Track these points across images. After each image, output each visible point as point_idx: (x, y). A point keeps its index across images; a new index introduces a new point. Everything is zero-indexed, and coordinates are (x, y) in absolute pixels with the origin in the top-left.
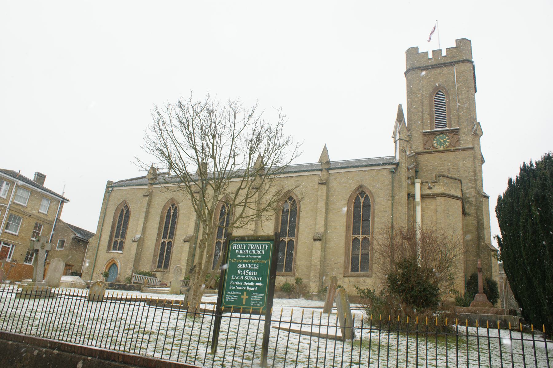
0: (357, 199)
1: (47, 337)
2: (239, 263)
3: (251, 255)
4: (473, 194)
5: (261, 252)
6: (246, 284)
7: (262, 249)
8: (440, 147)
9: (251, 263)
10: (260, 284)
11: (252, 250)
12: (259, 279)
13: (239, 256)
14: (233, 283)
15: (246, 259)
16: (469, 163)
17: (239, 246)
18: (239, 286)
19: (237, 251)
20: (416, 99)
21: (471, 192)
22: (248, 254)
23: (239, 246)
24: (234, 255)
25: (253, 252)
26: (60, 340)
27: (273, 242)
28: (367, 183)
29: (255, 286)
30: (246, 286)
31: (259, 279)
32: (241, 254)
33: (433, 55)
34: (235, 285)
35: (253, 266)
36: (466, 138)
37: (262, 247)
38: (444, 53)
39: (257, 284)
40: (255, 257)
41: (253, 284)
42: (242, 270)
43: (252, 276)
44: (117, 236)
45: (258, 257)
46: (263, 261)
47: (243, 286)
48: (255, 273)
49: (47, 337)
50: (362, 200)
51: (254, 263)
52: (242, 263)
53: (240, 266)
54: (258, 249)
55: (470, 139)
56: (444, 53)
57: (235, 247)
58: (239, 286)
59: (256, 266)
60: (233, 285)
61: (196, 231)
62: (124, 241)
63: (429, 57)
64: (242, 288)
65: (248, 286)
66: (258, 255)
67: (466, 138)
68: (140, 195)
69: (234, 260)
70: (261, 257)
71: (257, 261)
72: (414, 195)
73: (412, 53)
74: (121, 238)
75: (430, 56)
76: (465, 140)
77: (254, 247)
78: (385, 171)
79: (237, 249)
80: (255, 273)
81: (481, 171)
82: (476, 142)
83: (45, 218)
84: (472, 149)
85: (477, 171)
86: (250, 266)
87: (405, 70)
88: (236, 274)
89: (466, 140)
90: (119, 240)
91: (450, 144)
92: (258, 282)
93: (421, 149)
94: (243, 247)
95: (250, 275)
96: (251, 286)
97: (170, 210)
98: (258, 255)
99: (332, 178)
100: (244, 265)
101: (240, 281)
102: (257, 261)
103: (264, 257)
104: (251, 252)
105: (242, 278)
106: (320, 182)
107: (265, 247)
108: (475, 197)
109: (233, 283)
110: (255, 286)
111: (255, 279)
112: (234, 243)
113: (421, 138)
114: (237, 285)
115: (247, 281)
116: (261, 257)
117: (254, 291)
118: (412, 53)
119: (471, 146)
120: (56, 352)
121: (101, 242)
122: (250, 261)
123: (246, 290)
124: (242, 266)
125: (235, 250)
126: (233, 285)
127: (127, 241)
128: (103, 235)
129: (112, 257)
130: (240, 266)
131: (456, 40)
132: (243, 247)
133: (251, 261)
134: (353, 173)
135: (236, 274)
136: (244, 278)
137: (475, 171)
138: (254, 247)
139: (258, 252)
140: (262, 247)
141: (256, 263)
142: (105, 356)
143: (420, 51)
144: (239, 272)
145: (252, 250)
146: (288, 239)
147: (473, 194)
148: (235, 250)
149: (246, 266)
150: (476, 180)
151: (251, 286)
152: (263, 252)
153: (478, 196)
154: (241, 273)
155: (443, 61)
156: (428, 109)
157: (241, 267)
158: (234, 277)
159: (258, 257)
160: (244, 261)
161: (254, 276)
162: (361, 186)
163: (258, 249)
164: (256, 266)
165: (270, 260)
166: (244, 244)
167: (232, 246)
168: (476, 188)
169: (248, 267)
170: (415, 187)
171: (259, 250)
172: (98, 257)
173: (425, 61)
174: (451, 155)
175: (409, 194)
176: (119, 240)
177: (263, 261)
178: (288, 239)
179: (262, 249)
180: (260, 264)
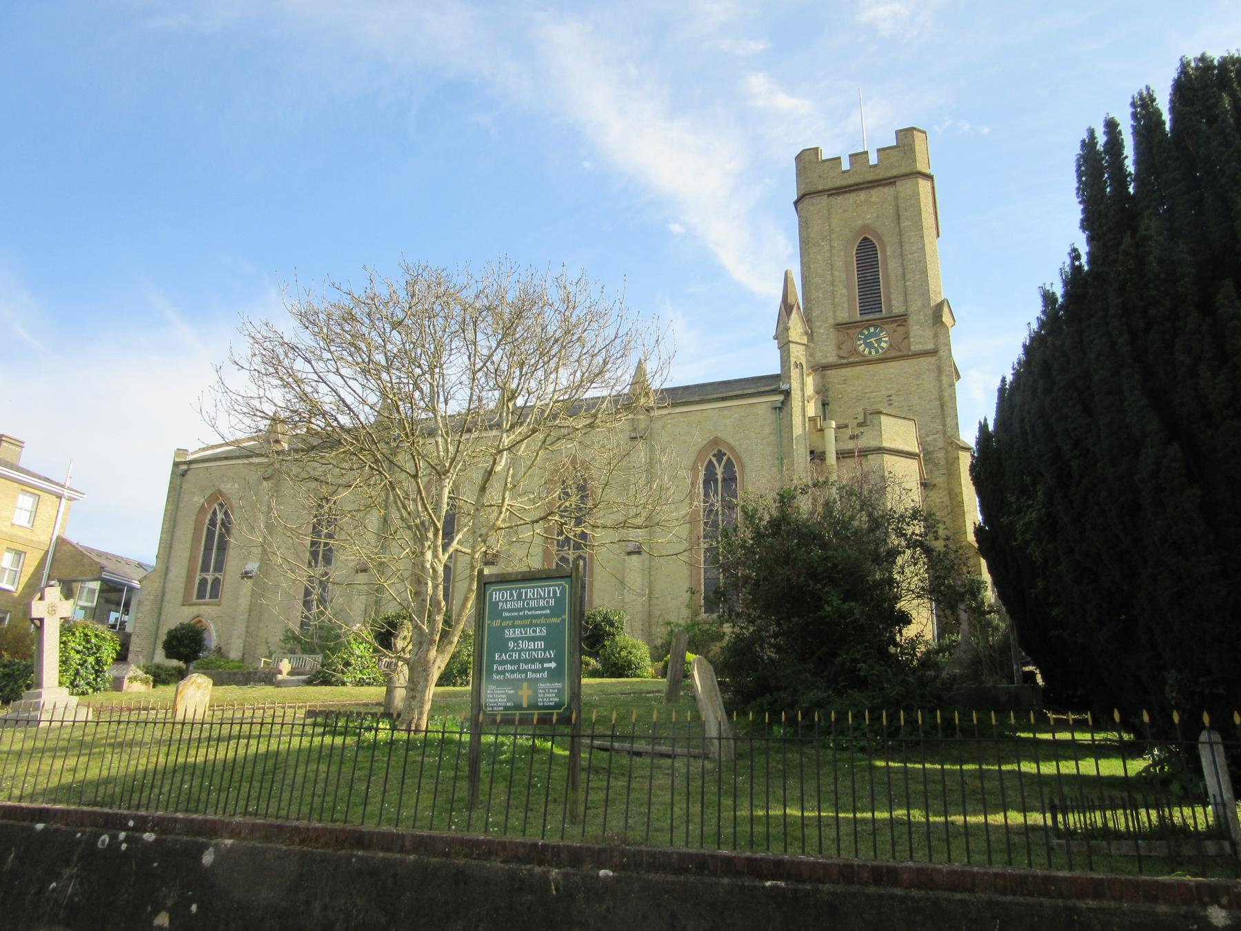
0: (710, 467)
1: (256, 814)
2: (509, 627)
3: (529, 609)
4: (941, 444)
5: (548, 603)
6: (525, 667)
7: (549, 597)
8: (870, 353)
9: (531, 626)
10: (553, 665)
11: (531, 599)
12: (550, 655)
13: (506, 614)
14: (500, 668)
15: (519, 618)
16: (929, 383)
17: (503, 594)
18: (512, 672)
19: (500, 604)
20: (819, 257)
21: (935, 440)
22: (524, 609)
23: (503, 594)
24: (496, 613)
25: (532, 604)
26: (250, 814)
27: (569, 580)
28: (229, 488)
29: (543, 670)
30: (525, 671)
31: (550, 655)
32: (509, 611)
33: (851, 164)
34: (503, 672)
35: (534, 631)
36: (922, 333)
37: (549, 592)
38: (873, 159)
39: (546, 665)
40: (538, 612)
41: (538, 666)
42: (516, 640)
43: (535, 650)
44: (205, 568)
45: (544, 612)
46: (554, 620)
47: (519, 671)
48: (541, 644)
49: (287, 818)
50: (719, 471)
51: (536, 625)
52: (514, 627)
53: (509, 633)
54: (541, 598)
55: (929, 333)
56: (873, 159)
57: (496, 596)
58: (512, 672)
59: (541, 630)
60: (499, 673)
61: (572, 632)
62: (221, 578)
63: (844, 169)
64: (519, 676)
65: (529, 670)
66: (543, 608)
67: (922, 333)
68: (253, 477)
69: (496, 623)
70: (548, 612)
71: (542, 620)
72: (824, 453)
73: (807, 161)
74: (215, 570)
75: (846, 166)
76: (920, 336)
77: (533, 594)
78: (764, 406)
79: (500, 601)
80: (541, 644)
81: (953, 398)
82: (942, 340)
83: (29, 537)
84: (934, 352)
85: (946, 399)
86: (530, 632)
87: (795, 198)
88: (505, 649)
89: (921, 336)
90: (210, 577)
91: (891, 345)
92: (549, 661)
93: (832, 359)
94: (511, 595)
95: (532, 650)
96: (534, 671)
97: (215, 513)
98: (543, 608)
99: (657, 425)
100: (517, 631)
101: (512, 662)
102: (542, 620)
103: (556, 611)
104: (528, 604)
105: (515, 656)
106: (633, 435)
107: (555, 592)
108: (943, 451)
109: (500, 668)
110: (543, 670)
111: (541, 655)
112: (494, 590)
113: (832, 336)
114: (508, 671)
115: (526, 662)
116: (548, 612)
117: (541, 680)
118: (807, 161)
119: (930, 346)
120: (40, 826)
121: (169, 585)
122: (527, 622)
123: (526, 679)
124: (515, 632)
125: (497, 603)
126: (499, 673)
127: (228, 578)
128: (171, 568)
129: (196, 613)
130: (509, 633)
131: (897, 132)
132: (511, 595)
133: (529, 620)
134: (699, 413)
135: (505, 649)
136: (520, 655)
137: (941, 398)
138: (533, 594)
139: (541, 603)
140: (549, 592)
141: (542, 625)
142: (408, 844)
143: (826, 155)
144: (511, 645)
145: (531, 599)
146: (574, 553)
147: (941, 444)
148: (497, 603)
149: (521, 632)
150: (943, 416)
151: (534, 671)
152: (552, 602)
153: (950, 448)
154: (514, 646)
155: (871, 177)
156: (844, 276)
157: (511, 636)
158: (500, 656)
159: (544, 612)
160: (517, 622)
161: (538, 650)
162: (716, 441)
163: (541, 598)
164: (541, 630)
165: (566, 617)
166: (513, 589)
167: (491, 595)
168: (945, 433)
169: (526, 633)
170: (823, 438)
171: (544, 599)
172: (163, 617)
173: (834, 177)
174: (892, 368)
175: (812, 452)
176: (210, 577)
177: (554, 620)
178: (574, 553)
179: (549, 597)
180: (548, 626)
